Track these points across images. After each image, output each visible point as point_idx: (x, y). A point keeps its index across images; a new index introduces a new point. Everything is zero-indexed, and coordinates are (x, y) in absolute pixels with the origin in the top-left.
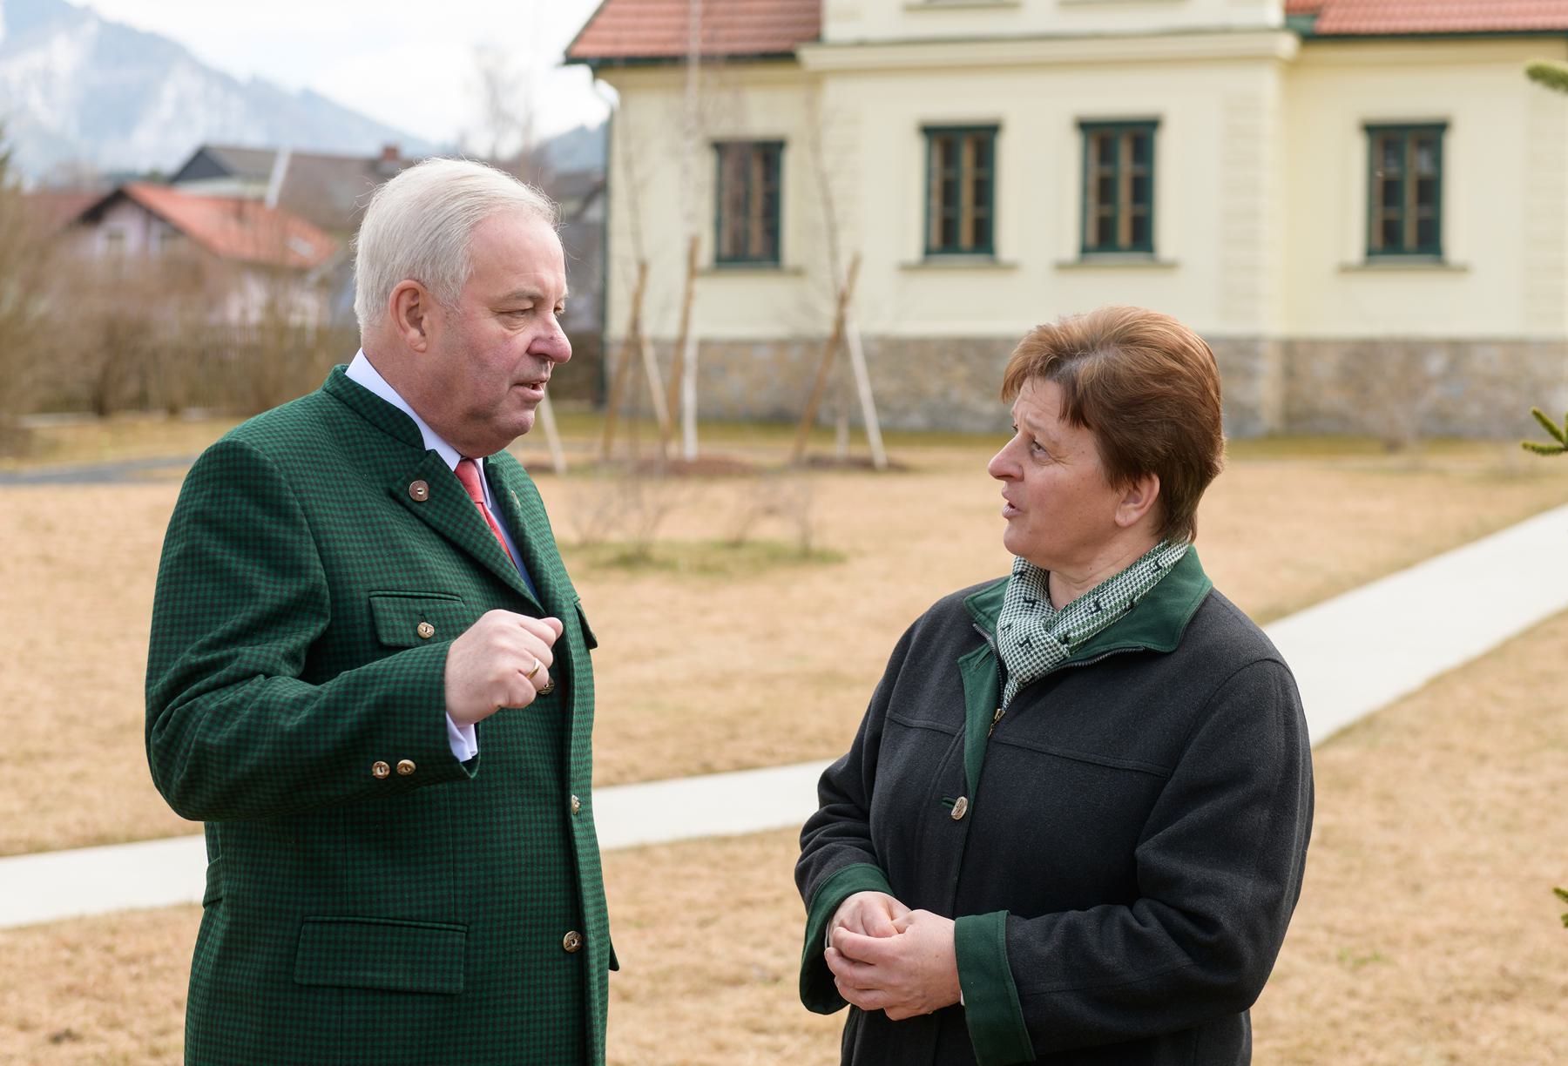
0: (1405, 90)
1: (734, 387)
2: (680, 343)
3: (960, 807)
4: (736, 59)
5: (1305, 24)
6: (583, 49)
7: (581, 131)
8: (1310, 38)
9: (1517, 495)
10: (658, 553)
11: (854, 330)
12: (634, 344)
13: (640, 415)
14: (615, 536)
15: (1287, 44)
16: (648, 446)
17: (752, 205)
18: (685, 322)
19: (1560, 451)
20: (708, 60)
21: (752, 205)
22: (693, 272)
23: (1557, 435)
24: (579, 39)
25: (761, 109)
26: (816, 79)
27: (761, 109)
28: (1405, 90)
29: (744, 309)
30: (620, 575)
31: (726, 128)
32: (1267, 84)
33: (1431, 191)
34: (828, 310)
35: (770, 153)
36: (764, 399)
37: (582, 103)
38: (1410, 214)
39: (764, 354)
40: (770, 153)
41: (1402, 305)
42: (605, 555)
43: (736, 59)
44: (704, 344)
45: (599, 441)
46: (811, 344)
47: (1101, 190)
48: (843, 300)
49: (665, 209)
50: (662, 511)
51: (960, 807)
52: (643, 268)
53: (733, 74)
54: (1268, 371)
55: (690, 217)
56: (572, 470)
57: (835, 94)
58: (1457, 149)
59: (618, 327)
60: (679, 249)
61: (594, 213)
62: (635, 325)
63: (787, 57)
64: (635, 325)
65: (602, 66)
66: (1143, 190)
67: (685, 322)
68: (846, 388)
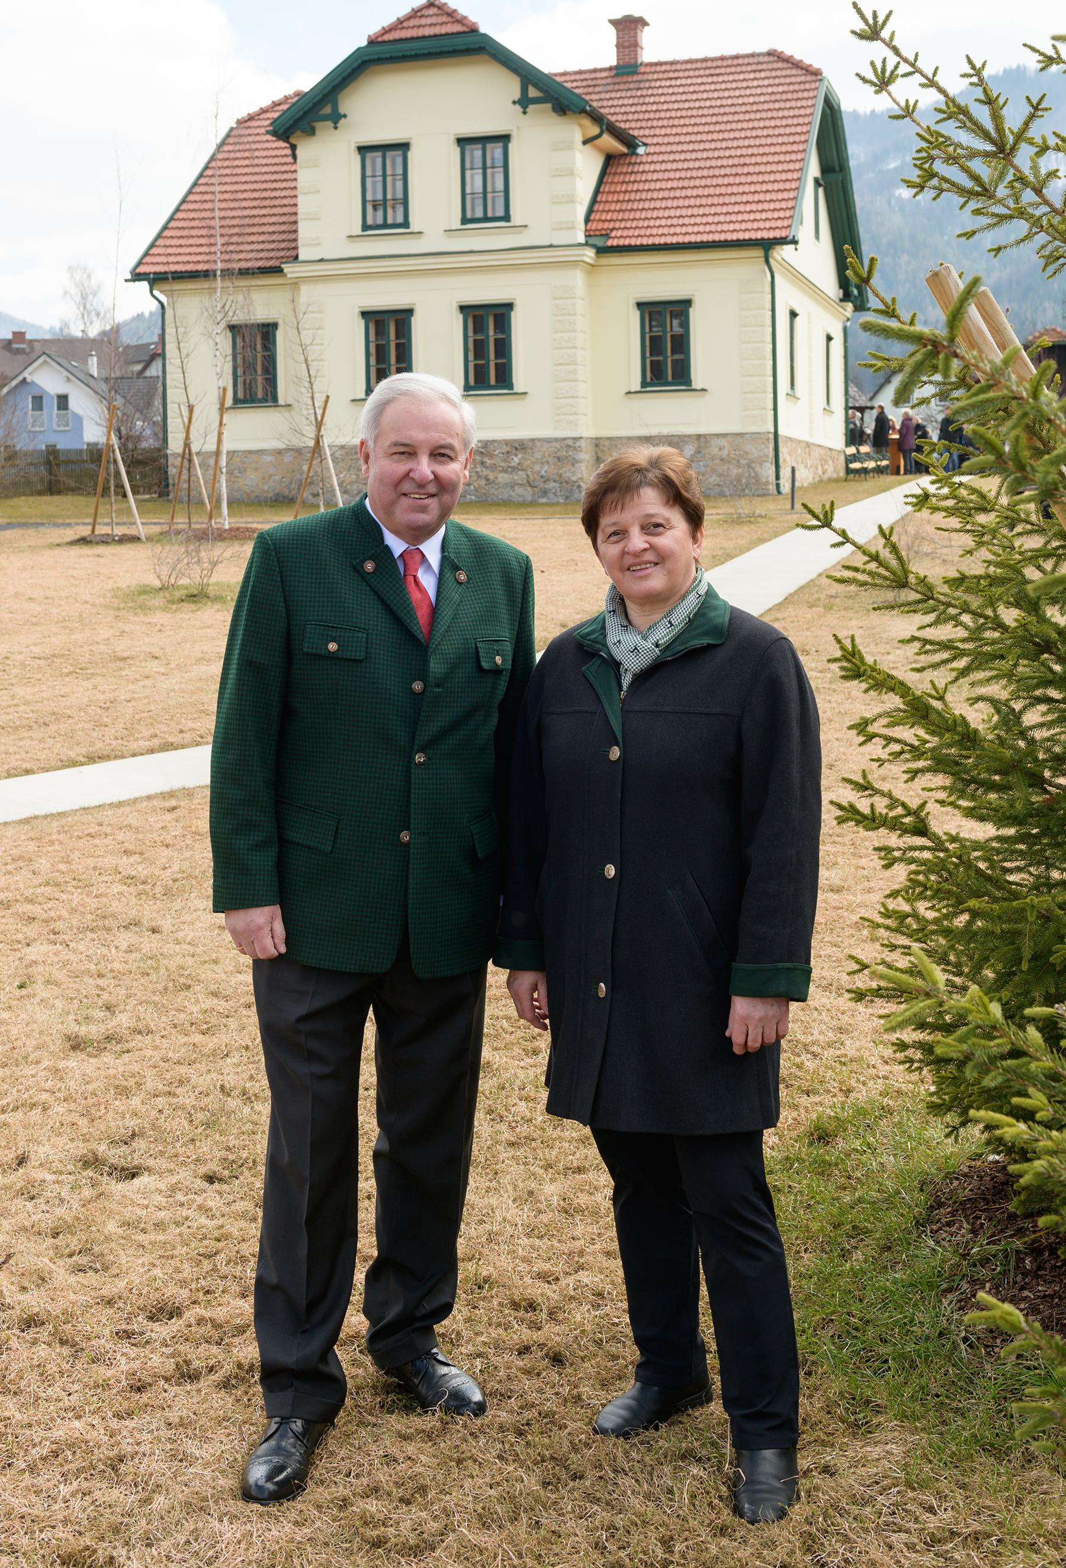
0: (663, 281)
1: (251, 481)
2: (218, 453)
3: (615, 753)
4: (244, 273)
5: (600, 242)
6: (142, 269)
7: (140, 317)
8: (602, 251)
9: (744, 532)
10: (211, 591)
11: (326, 442)
12: (187, 455)
13: (193, 502)
14: (184, 581)
15: (590, 254)
16: (200, 522)
17: (256, 367)
18: (219, 441)
19: (819, 527)
20: (227, 273)
21: (256, 367)
22: (222, 410)
23: (817, 518)
24: (140, 263)
25: (261, 304)
26: (295, 284)
27: (261, 304)
28: (663, 281)
29: (254, 431)
30: (188, 606)
31: (240, 317)
32: (578, 279)
33: (681, 343)
34: (310, 431)
35: (268, 331)
36: (269, 488)
37: (141, 300)
38: (669, 358)
39: (268, 458)
40: (268, 331)
41: (669, 414)
42: (178, 594)
43: (244, 273)
44: (231, 454)
45: (165, 518)
46: (298, 451)
47: (476, 349)
48: (319, 425)
49: (200, 370)
50: (214, 564)
51: (615, 753)
52: (191, 408)
53: (243, 282)
54: (586, 456)
55: (220, 376)
56: (149, 539)
57: (306, 292)
58: (697, 317)
59: (175, 445)
60: (214, 396)
61: (154, 370)
62: (187, 445)
63: (277, 271)
64: (187, 445)
65: (156, 280)
66: (504, 348)
67: (219, 441)
68: (324, 479)
